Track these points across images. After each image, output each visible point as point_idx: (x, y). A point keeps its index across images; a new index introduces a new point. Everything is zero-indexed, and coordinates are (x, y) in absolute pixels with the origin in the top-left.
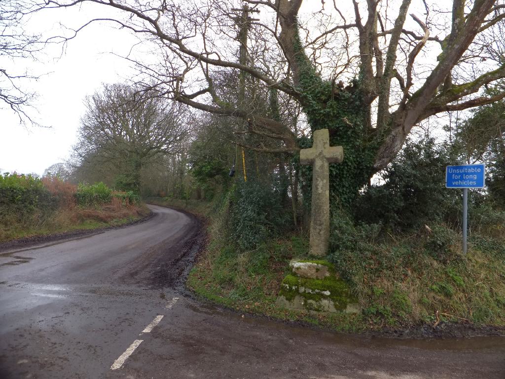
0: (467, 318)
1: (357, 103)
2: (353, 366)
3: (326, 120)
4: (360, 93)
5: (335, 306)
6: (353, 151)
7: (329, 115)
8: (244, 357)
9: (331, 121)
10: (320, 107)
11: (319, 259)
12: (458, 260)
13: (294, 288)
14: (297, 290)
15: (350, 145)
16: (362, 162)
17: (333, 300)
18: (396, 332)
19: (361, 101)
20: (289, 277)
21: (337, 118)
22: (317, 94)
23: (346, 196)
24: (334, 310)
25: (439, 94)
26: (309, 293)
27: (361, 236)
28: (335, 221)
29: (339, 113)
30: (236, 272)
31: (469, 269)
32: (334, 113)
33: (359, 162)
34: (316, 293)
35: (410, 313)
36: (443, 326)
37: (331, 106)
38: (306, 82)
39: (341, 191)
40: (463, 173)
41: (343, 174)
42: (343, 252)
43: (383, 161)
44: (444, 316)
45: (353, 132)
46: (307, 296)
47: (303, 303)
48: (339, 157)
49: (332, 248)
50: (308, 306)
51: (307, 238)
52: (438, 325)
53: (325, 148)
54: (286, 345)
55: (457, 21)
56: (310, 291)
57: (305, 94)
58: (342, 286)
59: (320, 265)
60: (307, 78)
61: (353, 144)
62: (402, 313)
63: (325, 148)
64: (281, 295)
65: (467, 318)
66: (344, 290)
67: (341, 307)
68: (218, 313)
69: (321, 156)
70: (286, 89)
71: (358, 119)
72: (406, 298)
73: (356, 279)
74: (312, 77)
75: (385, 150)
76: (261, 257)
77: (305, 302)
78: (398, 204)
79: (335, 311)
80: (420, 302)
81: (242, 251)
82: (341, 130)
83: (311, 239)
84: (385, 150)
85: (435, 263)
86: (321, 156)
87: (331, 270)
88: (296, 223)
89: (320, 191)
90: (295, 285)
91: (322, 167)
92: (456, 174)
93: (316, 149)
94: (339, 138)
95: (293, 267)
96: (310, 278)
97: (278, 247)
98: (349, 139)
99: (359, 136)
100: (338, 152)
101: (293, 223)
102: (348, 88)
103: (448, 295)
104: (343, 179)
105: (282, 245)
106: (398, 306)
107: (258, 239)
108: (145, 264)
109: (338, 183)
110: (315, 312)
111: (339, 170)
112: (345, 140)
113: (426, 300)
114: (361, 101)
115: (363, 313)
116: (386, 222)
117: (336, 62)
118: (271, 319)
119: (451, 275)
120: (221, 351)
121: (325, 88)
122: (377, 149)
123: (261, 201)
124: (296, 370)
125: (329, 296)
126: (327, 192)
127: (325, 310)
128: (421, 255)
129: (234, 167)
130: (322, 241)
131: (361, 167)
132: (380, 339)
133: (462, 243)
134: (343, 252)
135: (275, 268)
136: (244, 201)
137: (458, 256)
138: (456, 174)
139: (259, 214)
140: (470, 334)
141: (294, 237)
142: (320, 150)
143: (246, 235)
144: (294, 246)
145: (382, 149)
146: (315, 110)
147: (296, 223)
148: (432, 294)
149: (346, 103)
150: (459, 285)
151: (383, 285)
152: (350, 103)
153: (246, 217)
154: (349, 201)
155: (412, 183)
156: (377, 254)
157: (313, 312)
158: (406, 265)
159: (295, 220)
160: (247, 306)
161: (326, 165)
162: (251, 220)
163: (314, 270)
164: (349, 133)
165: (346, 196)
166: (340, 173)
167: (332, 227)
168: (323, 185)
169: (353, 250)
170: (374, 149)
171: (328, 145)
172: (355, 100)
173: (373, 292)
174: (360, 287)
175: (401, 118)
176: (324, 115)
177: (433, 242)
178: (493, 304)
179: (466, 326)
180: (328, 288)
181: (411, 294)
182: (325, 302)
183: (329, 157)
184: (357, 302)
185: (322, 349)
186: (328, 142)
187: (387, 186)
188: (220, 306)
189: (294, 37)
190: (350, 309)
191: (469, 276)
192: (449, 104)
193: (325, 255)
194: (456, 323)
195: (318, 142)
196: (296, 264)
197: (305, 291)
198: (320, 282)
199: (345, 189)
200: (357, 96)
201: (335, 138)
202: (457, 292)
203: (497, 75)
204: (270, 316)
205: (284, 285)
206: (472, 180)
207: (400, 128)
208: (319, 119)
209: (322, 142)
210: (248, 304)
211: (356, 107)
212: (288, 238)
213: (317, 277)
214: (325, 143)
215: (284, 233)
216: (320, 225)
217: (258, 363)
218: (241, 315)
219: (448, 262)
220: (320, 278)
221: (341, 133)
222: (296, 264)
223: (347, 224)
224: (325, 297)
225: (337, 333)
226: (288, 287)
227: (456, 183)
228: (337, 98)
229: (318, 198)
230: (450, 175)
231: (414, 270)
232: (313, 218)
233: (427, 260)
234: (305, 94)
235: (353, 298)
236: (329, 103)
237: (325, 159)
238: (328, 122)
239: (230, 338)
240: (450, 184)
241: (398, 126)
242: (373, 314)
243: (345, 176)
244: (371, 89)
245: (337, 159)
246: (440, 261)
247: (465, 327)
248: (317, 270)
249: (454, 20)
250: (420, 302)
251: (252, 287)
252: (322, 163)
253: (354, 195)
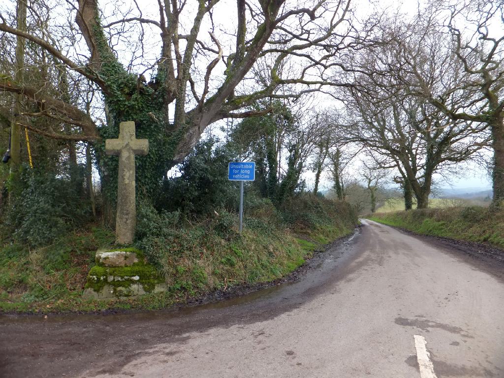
0: (245, 280)
1: (161, 100)
2: (170, 334)
3: (130, 112)
4: (163, 91)
5: (145, 289)
6: (155, 144)
7: (133, 108)
8: (63, 354)
9: (136, 114)
10: (124, 99)
11: (126, 247)
12: (238, 238)
13: (102, 278)
14: (106, 280)
15: (153, 139)
16: (163, 155)
17: (142, 284)
18: (197, 301)
19: (164, 98)
20: (96, 268)
21: (141, 111)
22: (119, 85)
23: (148, 187)
24: (144, 293)
25: (221, 103)
26: (119, 281)
27: (165, 223)
28: (143, 211)
29: (142, 107)
30: (28, 272)
31: (245, 243)
32: (139, 106)
33: (160, 155)
34: (125, 279)
35: (206, 284)
36: (229, 289)
37: (136, 99)
38: (108, 70)
39: (144, 182)
41: (146, 166)
42: (150, 238)
43: (182, 155)
44: (230, 281)
45: (155, 126)
46: (115, 284)
47: (112, 292)
48: (146, 150)
49: (139, 236)
50: (117, 294)
51: (114, 227)
52: (227, 289)
53: (131, 140)
54: (103, 332)
55: (240, 46)
56: (120, 279)
57: (109, 83)
58: (150, 270)
59: (128, 253)
60: (109, 66)
61: (155, 138)
62: (201, 285)
63: (131, 140)
64: (88, 288)
65: (245, 280)
66: (152, 273)
67: (149, 288)
68: (13, 321)
69: (128, 147)
70: (88, 74)
71: (160, 115)
72: (203, 272)
73: (163, 261)
74: (114, 66)
75: (184, 146)
76: (62, 252)
77: (115, 290)
78: (193, 193)
79: (144, 293)
80: (214, 273)
81: (33, 248)
82: (144, 124)
83: (117, 228)
84: (184, 146)
85: (223, 241)
86: (128, 147)
87: (139, 256)
88: (94, 214)
89: (127, 181)
90: (103, 276)
91: (129, 158)
93: (123, 140)
94: (142, 131)
95: (100, 258)
96: (118, 267)
97: (78, 239)
98: (152, 133)
99: (160, 130)
100: (144, 144)
101: (91, 214)
102: (151, 83)
103: (232, 265)
104: (146, 171)
105: (84, 238)
106: (197, 279)
107: (55, 233)
109: (140, 175)
110: (125, 298)
111: (142, 161)
112: (148, 133)
113: (218, 271)
114: (164, 98)
115: (170, 290)
116: (183, 210)
117: (138, 54)
118: (80, 313)
119: (234, 249)
120: (33, 356)
121: (128, 80)
122: (177, 144)
123: (56, 191)
124: (121, 350)
125: (138, 281)
126: (134, 183)
127: (135, 293)
128: (212, 236)
129: (8, 152)
130: (128, 230)
131: (162, 160)
132: (184, 309)
133: (239, 223)
134: (150, 238)
135: (78, 262)
136: (32, 192)
137: (238, 234)
138: (236, 169)
139: (53, 206)
140: (247, 292)
141: (94, 228)
142: (126, 142)
143: (39, 229)
144: (96, 238)
145: (181, 145)
146: (120, 101)
147: (94, 214)
148: (221, 266)
149: (150, 98)
150: (239, 256)
151: (185, 264)
152: (153, 99)
153: (37, 209)
154: (150, 191)
155: (204, 176)
156: (178, 238)
157: (123, 298)
158: (201, 245)
159: (94, 211)
160: (48, 306)
161: (133, 156)
162: (43, 213)
163: (123, 259)
164: (152, 127)
165: (148, 187)
166: (142, 164)
167: (139, 216)
168: (130, 176)
169: (158, 236)
170: (174, 144)
171: (134, 137)
172: (158, 97)
173: (177, 271)
174: (166, 268)
175: (198, 119)
176: (129, 107)
177: (221, 224)
178: (260, 267)
179: (245, 286)
180: (137, 273)
181: (205, 267)
182: (134, 287)
184: (164, 282)
185: (139, 327)
186: (135, 134)
187: (183, 176)
188: (12, 313)
189: (95, 19)
190: (158, 289)
191: (245, 249)
192: (231, 112)
193: (132, 242)
194: (238, 285)
195: (125, 134)
196: (103, 254)
197: (114, 279)
198: (129, 269)
199: (147, 180)
200: (161, 93)
201: (139, 130)
202: (238, 262)
203: (264, 95)
204: (78, 311)
205: (91, 277)
206: (246, 174)
207: (197, 128)
208: (124, 111)
209: (128, 134)
210: (49, 303)
211: (159, 104)
212: (89, 230)
213: (126, 264)
214: (132, 135)
215: (82, 225)
216: (127, 214)
217: (80, 355)
218: (43, 316)
219: (232, 239)
220: (129, 265)
221: (144, 126)
222: (103, 254)
223: (152, 212)
224: (134, 282)
225: (148, 311)
226: (96, 279)
228: (142, 92)
229: (125, 189)
231: (208, 249)
232: (119, 210)
233: (217, 239)
234: (109, 83)
235: (160, 278)
236: (134, 96)
238: (132, 114)
239: (38, 341)
240: (231, 177)
241: (195, 125)
242: (178, 289)
243: (147, 167)
244: (173, 89)
245: (143, 151)
246: (226, 239)
247: (244, 287)
248: (126, 258)
249: (238, 45)
250: (214, 273)
251: (52, 285)
252: (128, 155)
253: (155, 185)
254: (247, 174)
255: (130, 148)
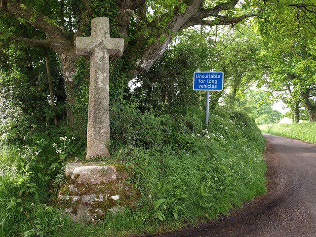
40: (207, 79)
91: (103, 58)
92: (201, 79)
108: (289, 93)
126: (108, 87)
138: (201, 79)
161: (107, 56)
171: (108, 36)
183: (110, 48)
195: (98, 31)
209: (102, 31)
227: (202, 86)
230: (197, 80)
237: (106, 51)
254: (215, 85)
255: (105, 48)
